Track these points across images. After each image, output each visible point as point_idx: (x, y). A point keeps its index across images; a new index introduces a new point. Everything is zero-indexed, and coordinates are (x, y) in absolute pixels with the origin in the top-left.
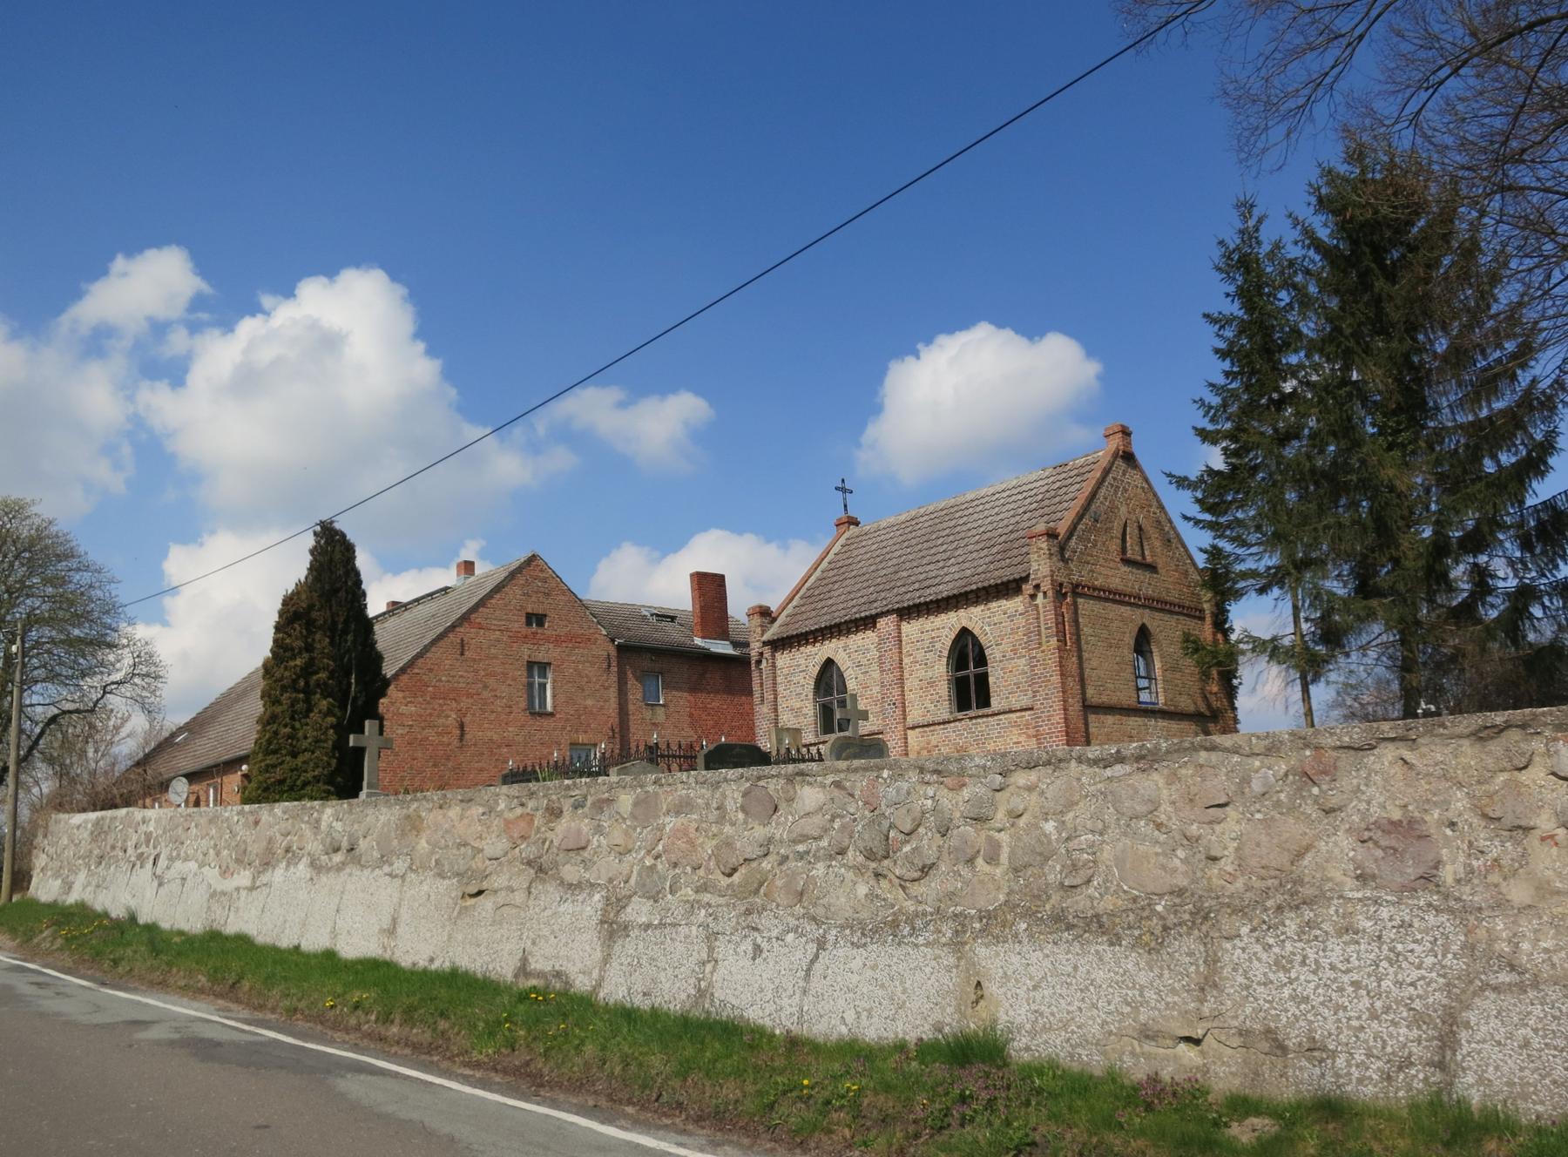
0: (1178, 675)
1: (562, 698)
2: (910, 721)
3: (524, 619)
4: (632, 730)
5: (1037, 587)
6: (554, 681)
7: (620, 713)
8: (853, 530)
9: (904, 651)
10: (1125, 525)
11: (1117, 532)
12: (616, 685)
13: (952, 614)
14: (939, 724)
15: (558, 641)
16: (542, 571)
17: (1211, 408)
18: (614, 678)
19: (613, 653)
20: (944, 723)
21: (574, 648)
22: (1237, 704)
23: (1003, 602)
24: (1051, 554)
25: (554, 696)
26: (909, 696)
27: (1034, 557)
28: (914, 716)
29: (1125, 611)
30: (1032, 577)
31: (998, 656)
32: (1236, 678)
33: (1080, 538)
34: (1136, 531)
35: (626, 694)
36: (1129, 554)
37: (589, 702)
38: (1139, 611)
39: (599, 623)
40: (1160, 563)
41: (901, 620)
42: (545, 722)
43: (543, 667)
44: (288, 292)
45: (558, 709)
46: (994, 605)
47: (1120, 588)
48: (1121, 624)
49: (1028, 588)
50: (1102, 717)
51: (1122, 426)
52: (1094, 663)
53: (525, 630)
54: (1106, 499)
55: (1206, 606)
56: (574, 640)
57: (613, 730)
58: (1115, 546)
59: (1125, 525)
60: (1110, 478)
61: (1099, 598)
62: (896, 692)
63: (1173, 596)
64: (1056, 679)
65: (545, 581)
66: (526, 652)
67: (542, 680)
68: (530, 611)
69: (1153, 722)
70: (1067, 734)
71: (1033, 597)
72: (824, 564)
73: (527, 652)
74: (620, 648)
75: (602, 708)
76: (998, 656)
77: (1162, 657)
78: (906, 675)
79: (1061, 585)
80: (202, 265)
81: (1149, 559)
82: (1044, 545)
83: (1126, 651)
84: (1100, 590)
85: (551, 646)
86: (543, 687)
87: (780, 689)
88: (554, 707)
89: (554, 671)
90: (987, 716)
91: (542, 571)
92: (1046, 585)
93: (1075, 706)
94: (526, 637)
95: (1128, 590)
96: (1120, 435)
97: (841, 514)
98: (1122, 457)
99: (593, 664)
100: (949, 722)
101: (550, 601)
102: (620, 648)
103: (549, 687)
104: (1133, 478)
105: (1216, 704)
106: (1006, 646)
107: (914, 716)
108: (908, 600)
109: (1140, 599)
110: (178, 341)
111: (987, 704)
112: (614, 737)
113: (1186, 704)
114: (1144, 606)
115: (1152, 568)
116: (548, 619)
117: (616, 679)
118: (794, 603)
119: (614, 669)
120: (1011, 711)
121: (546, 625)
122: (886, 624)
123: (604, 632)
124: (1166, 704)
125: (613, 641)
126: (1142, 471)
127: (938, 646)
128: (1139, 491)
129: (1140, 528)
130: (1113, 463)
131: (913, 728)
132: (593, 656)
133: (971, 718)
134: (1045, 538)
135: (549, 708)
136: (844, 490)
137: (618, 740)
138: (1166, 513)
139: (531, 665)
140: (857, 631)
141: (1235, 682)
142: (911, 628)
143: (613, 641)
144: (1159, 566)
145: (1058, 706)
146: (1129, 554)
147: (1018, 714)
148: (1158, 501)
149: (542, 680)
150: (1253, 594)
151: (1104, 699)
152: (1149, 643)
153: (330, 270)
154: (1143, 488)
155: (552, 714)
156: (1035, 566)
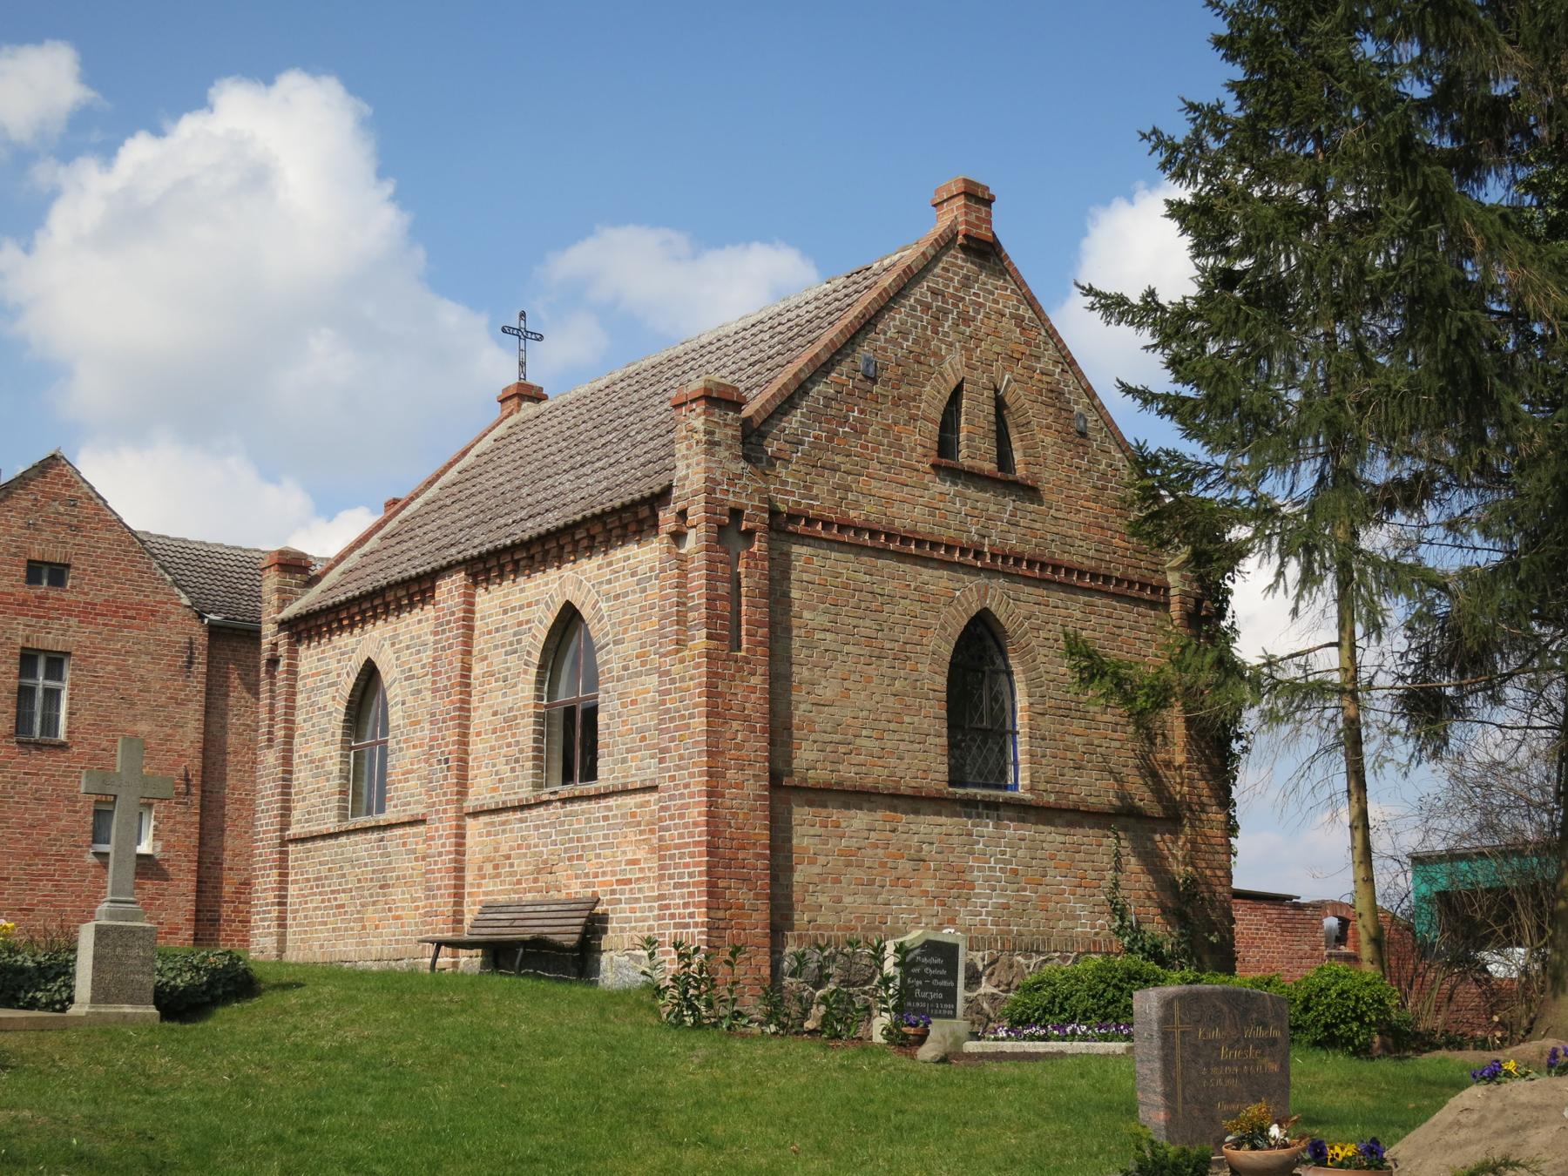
0: (1077, 726)
1: (86, 716)
2: (471, 803)
3: (22, 571)
4: (231, 781)
5: (683, 514)
6: (74, 686)
7: (204, 750)
8: (529, 409)
9: (475, 651)
10: (957, 393)
11: (932, 400)
12: (201, 697)
13: (552, 573)
14: (514, 809)
15: (88, 612)
16: (68, 485)
17: (1175, 149)
18: (197, 684)
19: (201, 638)
20: (522, 807)
21: (121, 627)
22: (1235, 794)
23: (632, 549)
24: (712, 443)
25: (71, 714)
26: (477, 746)
27: (681, 449)
28: (481, 791)
29: (936, 580)
30: (675, 493)
31: (616, 666)
32: (1239, 737)
33: (815, 416)
34: (989, 409)
35: (224, 715)
36: (964, 458)
37: (143, 727)
38: (973, 582)
39: (175, 583)
40: (1049, 479)
41: (476, 584)
42: (46, 760)
43: (55, 663)
44: (198, 101)
45: (78, 737)
46: (618, 554)
47: (923, 528)
48: (917, 608)
49: (667, 517)
50: (836, 814)
51: (965, 181)
52: (827, 691)
53: (24, 591)
54: (904, 334)
55: (1173, 579)
56: (123, 613)
57: (187, 780)
58: (921, 437)
59: (957, 393)
60: (921, 291)
61: (860, 549)
62: (452, 736)
63: (1083, 553)
64: (699, 723)
65: (73, 502)
66: (21, 632)
67: (52, 684)
68: (35, 556)
69: (990, 828)
70: (712, 849)
71: (678, 537)
72: (452, 475)
73: (21, 631)
74: (214, 631)
75: (168, 738)
76: (616, 666)
77: (1030, 682)
78: (475, 700)
79: (736, 513)
80: (90, 73)
81: (1020, 471)
82: (699, 423)
83: (924, 668)
84: (859, 530)
85: (73, 621)
86: (52, 696)
87: (300, 717)
88: (70, 733)
89: (76, 668)
90: (589, 798)
91: (68, 485)
92: (697, 512)
93: (747, 787)
94: (24, 603)
95: (946, 535)
96: (961, 201)
97: (510, 378)
98: (963, 248)
99: (156, 659)
100: (529, 807)
101: (78, 540)
102: (214, 631)
103: (64, 695)
104: (990, 293)
105: (1178, 788)
106: (630, 648)
107: (481, 791)
108: (481, 541)
109: (978, 554)
110: (44, 173)
111: (590, 774)
112: (188, 793)
113: (1094, 789)
114: (991, 572)
115: (1029, 491)
116: (72, 572)
117: (201, 687)
118: (366, 548)
119: (200, 668)
120: (625, 791)
121: (69, 583)
122: (450, 589)
123: (185, 601)
124: (1032, 789)
125: (201, 617)
126: (1020, 283)
127: (527, 639)
128: (1007, 323)
129: (1000, 404)
130: (936, 259)
131: (475, 814)
132: (158, 643)
133: (564, 801)
134: (699, 408)
135: (62, 735)
136: (523, 334)
137: (196, 800)
138: (1079, 375)
139: (28, 659)
140: (412, 605)
141: (1236, 746)
142: (489, 600)
143: (201, 617)
144: (1044, 487)
145: (699, 784)
146: (964, 458)
147: (639, 798)
148: (1060, 346)
149: (52, 684)
150: (1451, 573)
151: (848, 773)
152: (1003, 653)
153: (264, 73)
154: (1019, 320)
155: (63, 747)
156: (681, 472)
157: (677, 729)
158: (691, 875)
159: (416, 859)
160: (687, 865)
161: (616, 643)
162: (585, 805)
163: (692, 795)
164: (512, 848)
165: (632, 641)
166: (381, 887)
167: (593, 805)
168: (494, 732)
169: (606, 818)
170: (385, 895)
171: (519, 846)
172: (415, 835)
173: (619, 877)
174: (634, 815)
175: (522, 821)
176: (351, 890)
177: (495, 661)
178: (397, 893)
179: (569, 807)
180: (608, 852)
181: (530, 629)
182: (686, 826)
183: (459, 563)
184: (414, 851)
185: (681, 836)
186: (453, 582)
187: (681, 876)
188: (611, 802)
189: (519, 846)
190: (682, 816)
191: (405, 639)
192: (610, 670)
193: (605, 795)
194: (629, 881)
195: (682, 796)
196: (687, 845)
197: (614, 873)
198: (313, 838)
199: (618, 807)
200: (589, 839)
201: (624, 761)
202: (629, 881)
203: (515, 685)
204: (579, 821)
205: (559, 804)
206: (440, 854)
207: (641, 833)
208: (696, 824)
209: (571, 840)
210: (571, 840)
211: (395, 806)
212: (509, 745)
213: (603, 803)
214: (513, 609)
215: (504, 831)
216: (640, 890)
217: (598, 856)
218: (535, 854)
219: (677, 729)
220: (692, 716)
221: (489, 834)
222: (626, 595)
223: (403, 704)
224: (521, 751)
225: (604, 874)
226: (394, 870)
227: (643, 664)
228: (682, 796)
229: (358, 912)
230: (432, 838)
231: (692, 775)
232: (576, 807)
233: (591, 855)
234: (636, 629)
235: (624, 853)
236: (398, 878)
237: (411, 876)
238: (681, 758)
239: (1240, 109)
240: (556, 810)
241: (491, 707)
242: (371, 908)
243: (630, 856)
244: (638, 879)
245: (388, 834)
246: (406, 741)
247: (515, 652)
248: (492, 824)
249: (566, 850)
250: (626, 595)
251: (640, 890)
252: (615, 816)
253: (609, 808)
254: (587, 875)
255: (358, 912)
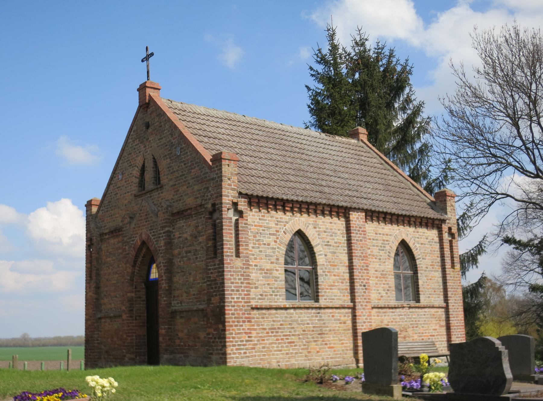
14: (389, 308)
31: (424, 267)
157: (454, 291)
158: (461, 334)
159: (340, 323)
160: (459, 332)
161: (423, 259)
162: (417, 310)
163: (459, 312)
164: (389, 322)
165: (429, 260)
166: (319, 334)
167: (420, 310)
168: (377, 277)
169: (424, 315)
170: (322, 338)
171: (392, 322)
172: (339, 313)
173: (430, 334)
174: (434, 315)
175: (393, 312)
176: (299, 335)
177: (374, 251)
178: (330, 338)
179: (411, 310)
180: (426, 326)
181: (389, 244)
182: (458, 320)
183: (363, 209)
184: (339, 320)
185: (457, 323)
186: (359, 215)
187: (458, 335)
188: (426, 310)
189: (392, 322)
190: (457, 317)
191: (323, 228)
192: (422, 267)
193: (424, 308)
194: (434, 336)
195: (456, 311)
196: (459, 326)
197: (429, 333)
198: (261, 309)
199: (429, 312)
200: (419, 321)
201: (429, 297)
202: (434, 336)
203: (384, 262)
204: (415, 315)
205: (407, 308)
206: (365, 322)
207: (437, 321)
208: (461, 320)
209: (412, 321)
210: (412, 321)
211: (325, 299)
212: (384, 284)
213: (423, 310)
214: (380, 234)
215: (385, 316)
216: (438, 338)
217: (423, 327)
218: (399, 325)
219: (454, 291)
220: (457, 288)
221: (378, 316)
222: (425, 244)
223: (326, 255)
224: (390, 287)
225: (426, 333)
226: (327, 327)
227: (433, 268)
228: (456, 311)
229: (305, 345)
230: (368, 316)
231: (459, 306)
232: (413, 310)
233: (420, 326)
234: (429, 256)
235: (431, 326)
236: (330, 331)
237: (338, 330)
238: (455, 300)
239: (323, 86)
240: (406, 310)
241: (374, 268)
242: (313, 344)
243: (434, 328)
244: (437, 335)
245: (322, 311)
246: (329, 272)
247: (383, 250)
248: (380, 312)
249: (411, 324)
250: (425, 244)
251: (438, 338)
252: (428, 315)
253: (426, 312)
254: (419, 333)
255: (305, 345)
